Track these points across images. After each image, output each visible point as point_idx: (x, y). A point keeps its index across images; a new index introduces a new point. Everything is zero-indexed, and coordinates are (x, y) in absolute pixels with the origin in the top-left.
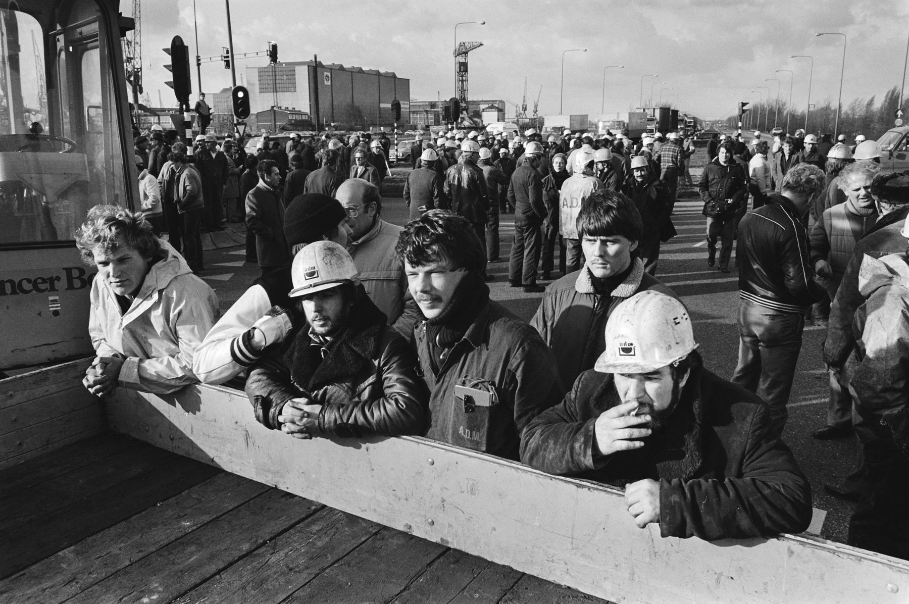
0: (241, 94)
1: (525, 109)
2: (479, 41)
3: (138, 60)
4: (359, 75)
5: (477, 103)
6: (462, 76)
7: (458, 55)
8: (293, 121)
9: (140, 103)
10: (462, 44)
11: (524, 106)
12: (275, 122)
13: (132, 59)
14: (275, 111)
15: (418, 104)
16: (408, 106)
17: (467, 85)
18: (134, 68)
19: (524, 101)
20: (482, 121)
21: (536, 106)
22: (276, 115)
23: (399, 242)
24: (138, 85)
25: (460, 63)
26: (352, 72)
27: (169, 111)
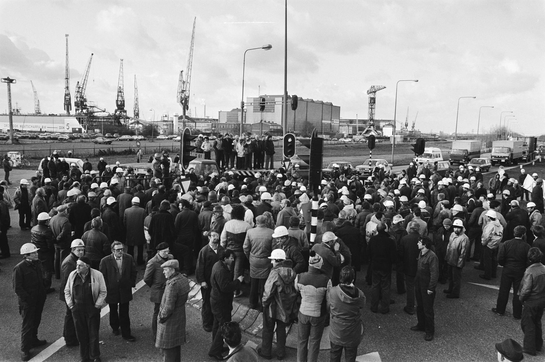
0: (290, 140)
1: (406, 125)
2: (384, 85)
3: (187, 92)
4: (311, 103)
5: (379, 121)
6: (372, 106)
7: (370, 93)
8: (272, 130)
9: (186, 115)
10: (373, 87)
11: (406, 124)
12: (262, 130)
13: (184, 91)
14: (262, 123)
15: (342, 120)
16: (339, 122)
17: (374, 111)
18: (185, 96)
19: (406, 120)
20: (383, 133)
21: (414, 124)
22: (263, 126)
23: (404, 235)
24: (186, 105)
25: (371, 98)
26: (307, 102)
27: (201, 120)
